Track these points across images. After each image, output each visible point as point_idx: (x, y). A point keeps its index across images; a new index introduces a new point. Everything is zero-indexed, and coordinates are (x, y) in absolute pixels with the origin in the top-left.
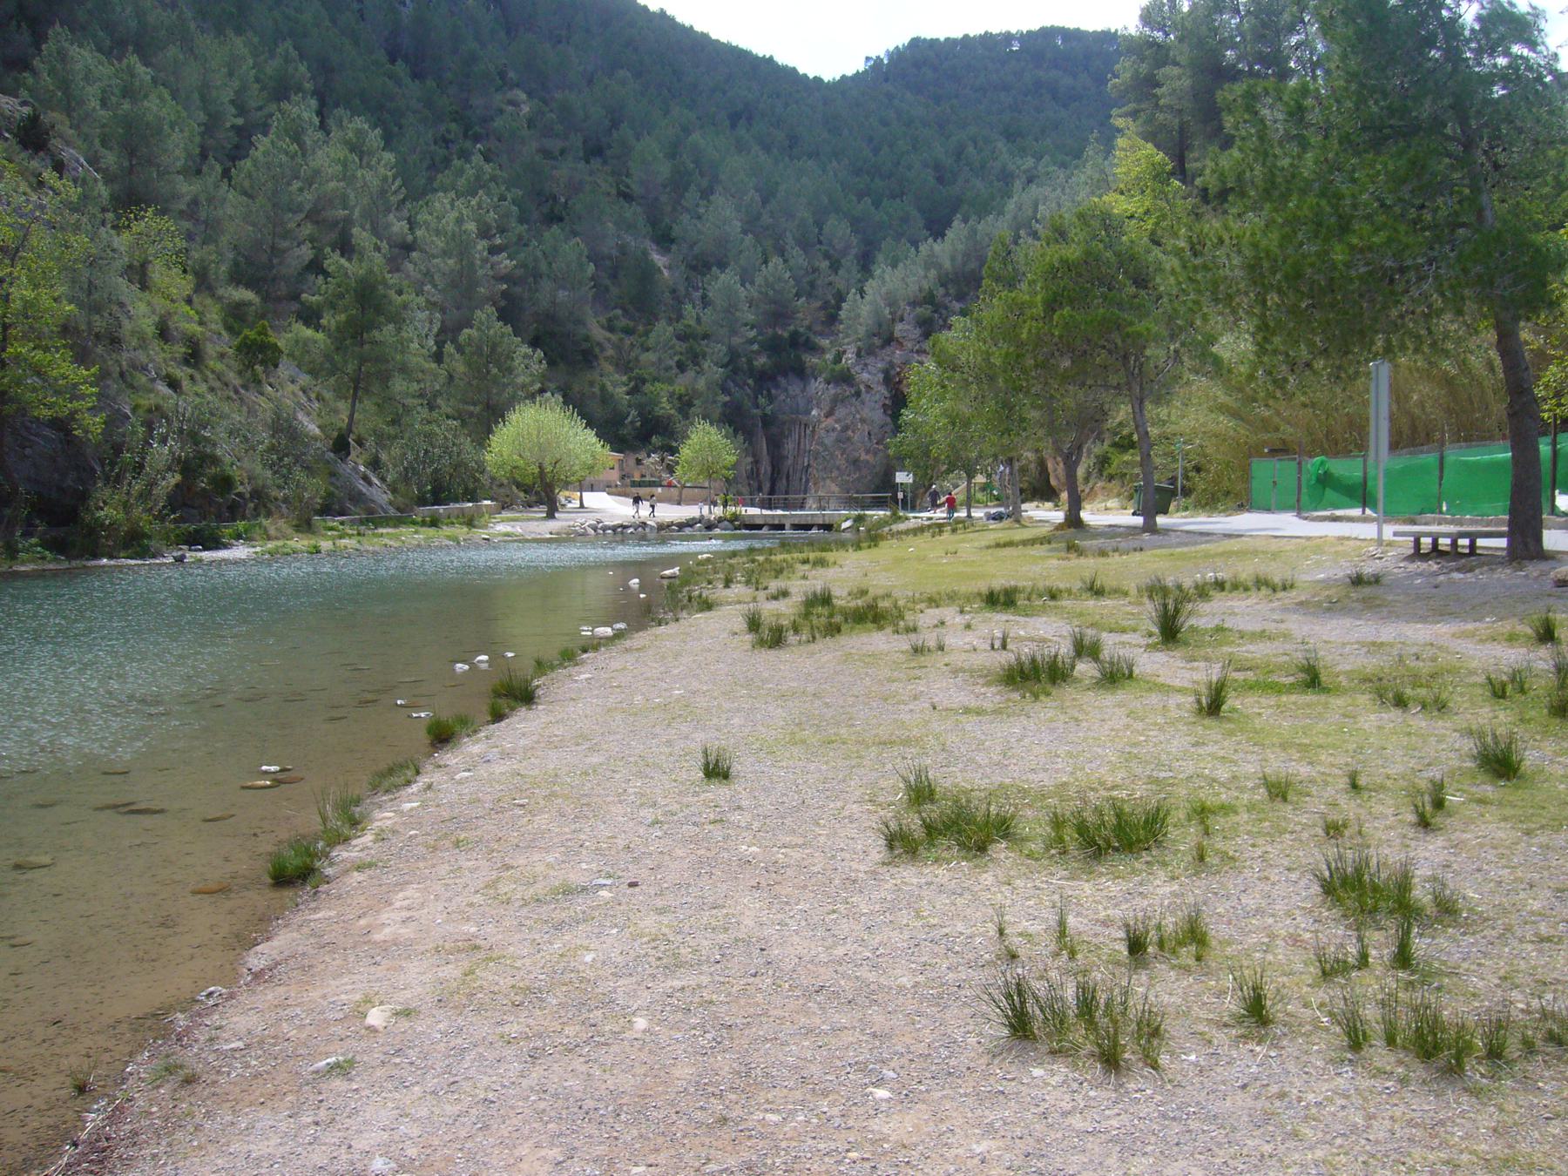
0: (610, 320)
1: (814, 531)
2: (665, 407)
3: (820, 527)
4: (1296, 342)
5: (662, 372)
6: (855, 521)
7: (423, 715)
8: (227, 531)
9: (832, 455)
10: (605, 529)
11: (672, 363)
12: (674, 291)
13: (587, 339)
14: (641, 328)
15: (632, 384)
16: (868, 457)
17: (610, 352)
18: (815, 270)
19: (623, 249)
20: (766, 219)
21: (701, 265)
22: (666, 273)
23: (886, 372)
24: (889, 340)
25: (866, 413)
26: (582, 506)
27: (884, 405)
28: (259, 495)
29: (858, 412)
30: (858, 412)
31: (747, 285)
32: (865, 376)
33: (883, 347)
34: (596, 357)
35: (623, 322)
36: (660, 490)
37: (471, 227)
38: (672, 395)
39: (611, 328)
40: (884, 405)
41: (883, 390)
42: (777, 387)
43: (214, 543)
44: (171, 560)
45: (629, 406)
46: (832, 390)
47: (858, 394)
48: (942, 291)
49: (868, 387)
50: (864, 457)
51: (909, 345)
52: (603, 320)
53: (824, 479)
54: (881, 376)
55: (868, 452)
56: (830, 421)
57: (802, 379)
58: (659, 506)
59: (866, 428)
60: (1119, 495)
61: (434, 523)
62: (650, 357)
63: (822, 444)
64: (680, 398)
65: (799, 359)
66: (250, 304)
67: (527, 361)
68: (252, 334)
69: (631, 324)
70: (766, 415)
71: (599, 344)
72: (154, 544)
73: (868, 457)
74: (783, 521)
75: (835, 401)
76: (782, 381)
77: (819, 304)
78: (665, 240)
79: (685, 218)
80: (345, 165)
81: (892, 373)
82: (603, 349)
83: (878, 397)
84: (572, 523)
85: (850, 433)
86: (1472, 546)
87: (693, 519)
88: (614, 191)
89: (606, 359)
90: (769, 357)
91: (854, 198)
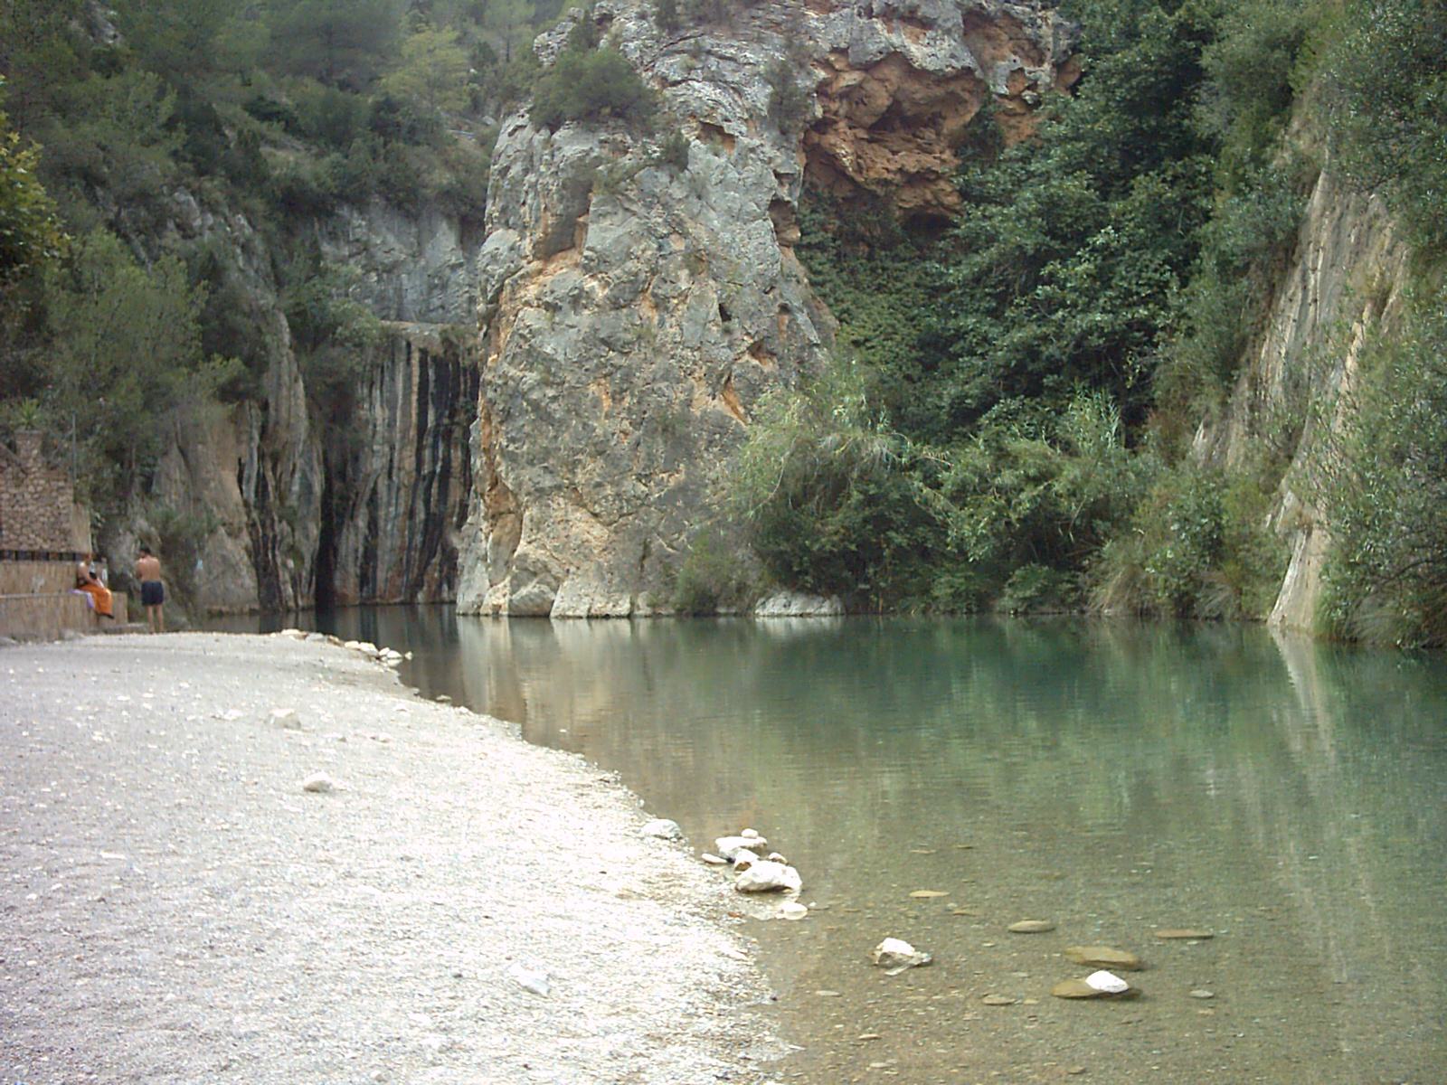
4: (1071, 35)
9: (573, 396)
16: (718, 405)
23: (780, 78)
27: (776, 204)
28: (479, 595)
29: (678, 228)
40: (776, 204)
41: (762, 142)
46: (572, 145)
47: (676, 158)
49: (713, 132)
54: (760, 95)
55: (721, 382)
56: (563, 274)
58: (649, 621)
63: (533, 357)
73: (718, 405)
83: (754, 169)
85: (645, 309)
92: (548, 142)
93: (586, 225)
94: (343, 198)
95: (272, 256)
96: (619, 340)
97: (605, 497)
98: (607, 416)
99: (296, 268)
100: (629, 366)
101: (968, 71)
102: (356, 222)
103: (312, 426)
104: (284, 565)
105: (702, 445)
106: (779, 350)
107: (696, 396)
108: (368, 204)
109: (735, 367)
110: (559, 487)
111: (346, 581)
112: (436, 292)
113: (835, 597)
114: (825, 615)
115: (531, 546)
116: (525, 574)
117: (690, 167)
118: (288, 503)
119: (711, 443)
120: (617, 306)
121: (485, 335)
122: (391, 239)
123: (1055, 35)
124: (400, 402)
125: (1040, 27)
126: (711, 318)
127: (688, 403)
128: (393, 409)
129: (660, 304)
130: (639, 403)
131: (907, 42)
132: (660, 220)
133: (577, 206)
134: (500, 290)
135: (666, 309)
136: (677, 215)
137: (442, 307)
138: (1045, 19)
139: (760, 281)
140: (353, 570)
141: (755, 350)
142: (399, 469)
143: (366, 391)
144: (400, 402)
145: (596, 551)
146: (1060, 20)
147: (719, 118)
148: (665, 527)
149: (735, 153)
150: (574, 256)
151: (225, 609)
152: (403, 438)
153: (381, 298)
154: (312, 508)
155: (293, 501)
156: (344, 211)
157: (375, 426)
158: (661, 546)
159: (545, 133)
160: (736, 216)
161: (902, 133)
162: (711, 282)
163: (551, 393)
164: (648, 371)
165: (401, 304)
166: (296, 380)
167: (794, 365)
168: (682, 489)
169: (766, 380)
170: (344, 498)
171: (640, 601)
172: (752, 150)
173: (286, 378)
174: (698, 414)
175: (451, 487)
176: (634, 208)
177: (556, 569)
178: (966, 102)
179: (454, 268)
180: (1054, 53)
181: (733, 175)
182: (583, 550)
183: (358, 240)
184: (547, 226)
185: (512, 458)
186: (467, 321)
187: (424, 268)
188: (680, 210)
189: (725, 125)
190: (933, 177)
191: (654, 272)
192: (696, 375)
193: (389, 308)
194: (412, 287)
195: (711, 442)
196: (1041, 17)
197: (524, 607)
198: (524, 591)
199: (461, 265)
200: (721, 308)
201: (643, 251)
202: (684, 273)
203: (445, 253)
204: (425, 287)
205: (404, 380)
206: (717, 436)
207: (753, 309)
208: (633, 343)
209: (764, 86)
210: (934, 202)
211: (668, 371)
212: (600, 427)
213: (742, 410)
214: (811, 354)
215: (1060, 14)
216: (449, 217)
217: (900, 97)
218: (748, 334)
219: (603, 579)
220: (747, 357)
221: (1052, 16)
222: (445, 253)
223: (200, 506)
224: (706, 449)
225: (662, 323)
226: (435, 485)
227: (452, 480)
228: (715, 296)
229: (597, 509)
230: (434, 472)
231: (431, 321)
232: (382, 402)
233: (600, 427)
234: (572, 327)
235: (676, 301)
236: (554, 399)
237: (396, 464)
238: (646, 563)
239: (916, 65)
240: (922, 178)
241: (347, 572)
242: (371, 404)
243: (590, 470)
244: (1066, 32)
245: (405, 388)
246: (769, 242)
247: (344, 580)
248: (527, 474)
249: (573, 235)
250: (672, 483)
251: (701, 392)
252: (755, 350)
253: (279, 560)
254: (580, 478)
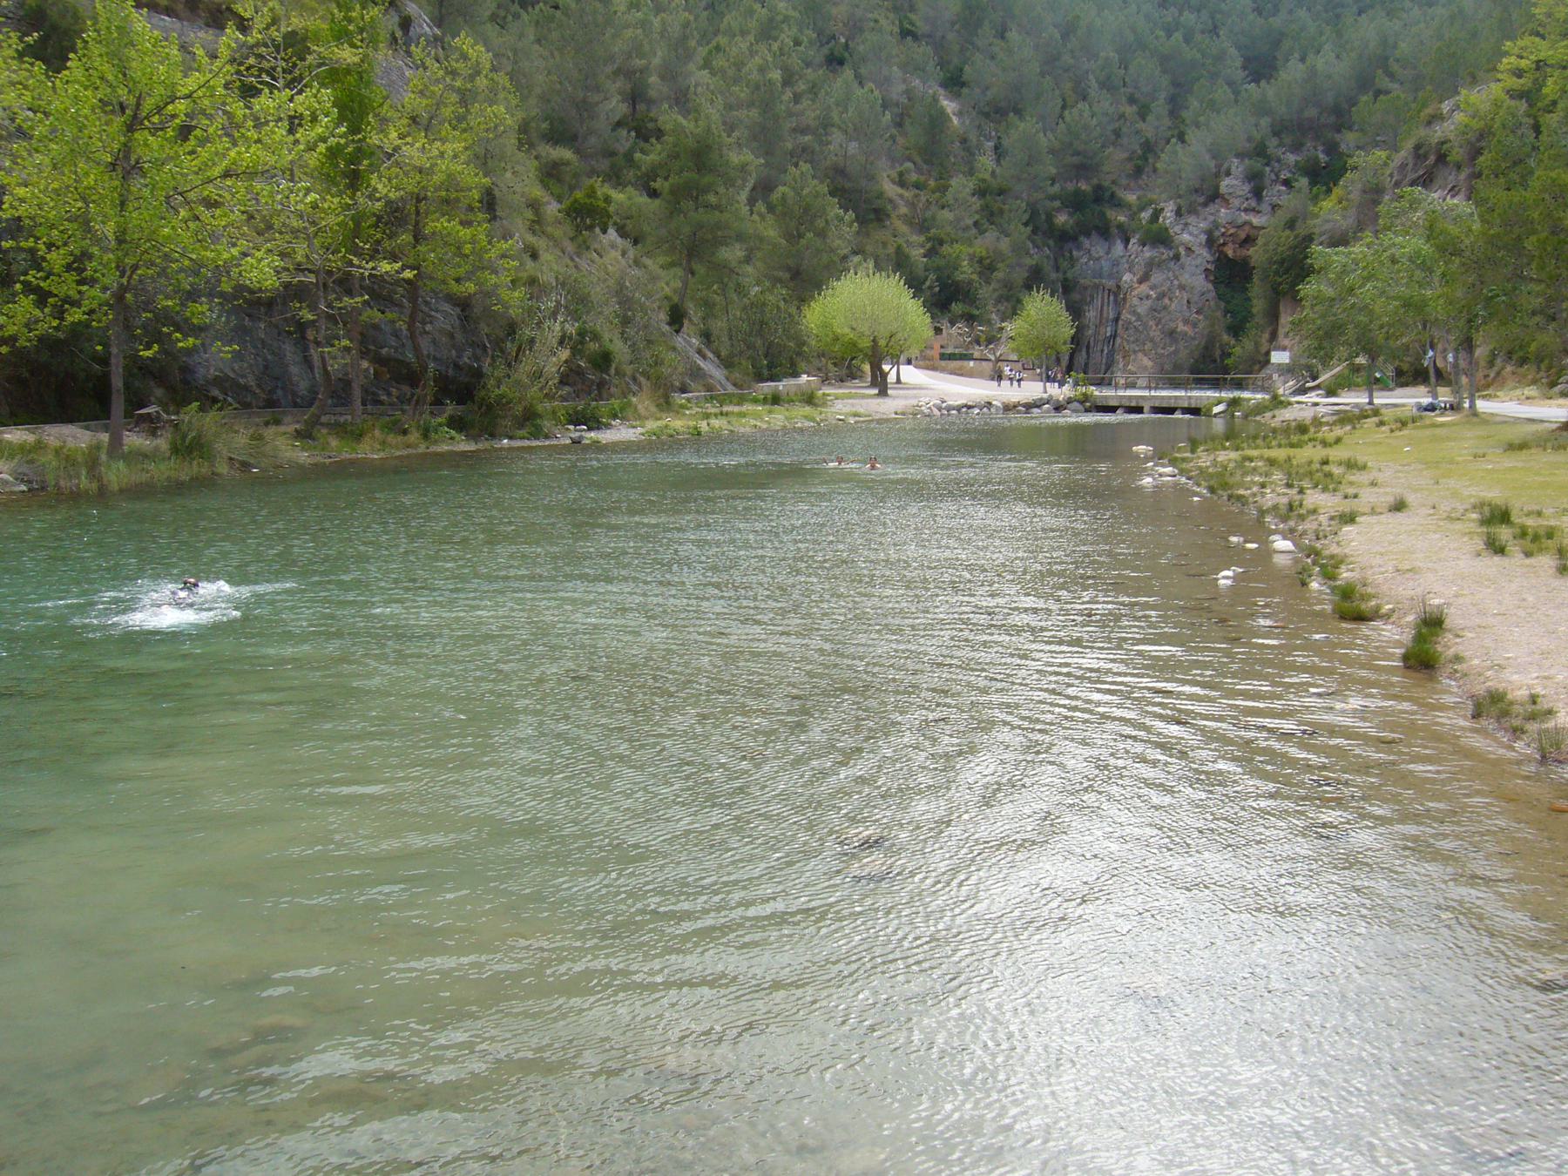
0: (901, 174)
1: (1178, 416)
2: (966, 272)
3: (1186, 411)
5: (960, 232)
6: (1228, 405)
7: (49, 604)
8: (603, 407)
9: (1145, 325)
10: (949, 408)
11: (970, 222)
12: (964, 141)
13: (880, 195)
14: (932, 183)
15: (929, 245)
16: (1186, 328)
17: (904, 210)
18: (1122, 116)
19: (909, 93)
20: (1067, 59)
21: (998, 112)
22: (955, 120)
23: (1209, 233)
24: (1214, 196)
25: (1185, 278)
26: (898, 381)
27: (1206, 270)
29: (1176, 278)
30: (1176, 278)
31: (1048, 133)
32: (1186, 237)
33: (1205, 205)
34: (888, 216)
35: (914, 177)
36: (972, 363)
37: (776, 75)
38: (972, 257)
39: (902, 183)
40: (1206, 270)
41: (1205, 253)
42: (1079, 248)
43: (594, 423)
44: (568, 441)
45: (926, 270)
46: (1148, 253)
47: (1177, 257)
48: (1274, 142)
49: (1188, 249)
50: (1181, 327)
51: (1236, 202)
52: (894, 175)
53: (1135, 352)
54: (1203, 238)
55: (1186, 322)
56: (1144, 288)
57: (1106, 239)
60: (1534, 382)
61: (776, 400)
62: (946, 215)
63: (1134, 313)
64: (981, 261)
65: (1103, 214)
66: (568, 163)
67: (842, 227)
68: (579, 194)
69: (922, 178)
70: (1066, 280)
71: (891, 201)
72: (547, 424)
73: (1186, 328)
74: (1141, 404)
75: (1151, 265)
76: (1086, 242)
77: (1125, 155)
78: (954, 83)
79: (978, 57)
81: (1217, 233)
82: (895, 207)
83: (1199, 261)
84: (915, 402)
85: (1166, 301)
87: (1041, 399)
88: (896, 30)
89: (899, 217)
90: (1070, 214)
91: (1162, 33)
99: (1064, 264)
129: (1170, 299)
141: (1197, 313)
150: (1148, 283)
156: (1082, 239)
185: (1128, 341)
212: (1152, 334)
233: (1152, 334)
243: (1148, 346)
248: (1133, 346)
252: (1197, 313)
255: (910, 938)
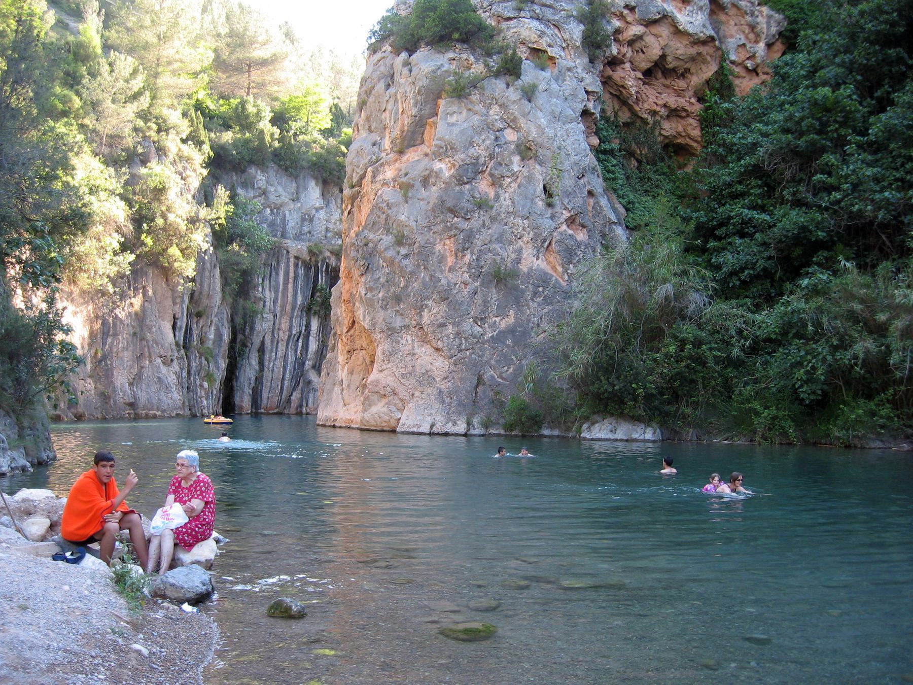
9: (425, 254)
27: (585, 113)
29: (512, 124)
30: (512, 124)
40: (585, 113)
54: (576, 31)
55: (543, 245)
59: (539, 174)
73: (541, 264)
76: (260, 178)
80: (128, 30)
83: (570, 83)
85: (483, 186)
86: (838, 135)
92: (406, 64)
93: (435, 123)
94: (251, 162)
95: (205, 192)
96: (463, 208)
97: (448, 336)
98: (451, 270)
100: (471, 229)
101: (712, 39)
102: (259, 177)
103: (223, 299)
104: (201, 386)
105: (529, 295)
106: (588, 223)
107: (524, 256)
108: (267, 168)
109: (555, 234)
110: (407, 327)
111: (244, 400)
112: (306, 223)
113: (654, 424)
114: (648, 441)
115: (382, 374)
116: (376, 396)
117: (521, 77)
118: (206, 346)
119: (535, 294)
120: (461, 183)
121: (349, 213)
122: (280, 189)
123: (768, 23)
124: (281, 288)
125: (757, 16)
126: (538, 193)
127: (518, 261)
128: (276, 292)
129: (496, 182)
130: (478, 259)
131: (675, 11)
132: (497, 118)
133: (427, 110)
134: (363, 176)
135: (501, 186)
136: (513, 114)
137: (310, 232)
138: (761, 12)
139: (576, 168)
140: (248, 391)
141: (571, 221)
142: (279, 329)
143: (260, 280)
144: (281, 288)
145: (437, 379)
146: (772, 13)
147: (544, 44)
148: (496, 361)
149: (556, 71)
151: (158, 413)
152: (282, 310)
153: (272, 225)
154: (222, 349)
155: (210, 344)
156: (252, 170)
157: (265, 302)
158: (492, 377)
159: (404, 55)
160: (556, 117)
161: (663, 80)
162: (538, 167)
163: (403, 251)
164: (485, 235)
165: (284, 228)
166: (215, 267)
167: (598, 237)
168: (511, 331)
169: (579, 247)
170: (244, 345)
171: (476, 421)
172: (569, 69)
173: (208, 265)
174: (525, 270)
175: (310, 343)
176: (476, 108)
177: (402, 393)
178: (709, 63)
179: (317, 210)
180: (767, 35)
181: (555, 86)
182: (426, 378)
183: (260, 188)
184: (403, 125)
186: (324, 242)
187: (299, 209)
188: (514, 109)
189: (549, 49)
190: (684, 114)
191: (491, 157)
192: (525, 239)
193: (277, 231)
194: (292, 221)
195: (536, 293)
196: (758, 11)
197: (373, 423)
198: (374, 409)
199: (322, 208)
200: (545, 188)
201: (484, 141)
202: (516, 159)
203: (313, 200)
204: (299, 220)
205: (287, 271)
206: (541, 289)
207: (570, 190)
208: (474, 212)
209: (578, 25)
210: (683, 134)
211: (502, 235)
212: (445, 278)
213: (560, 269)
214: (611, 230)
215: (772, 8)
216: (316, 178)
217: (668, 52)
218: (566, 209)
219: (443, 402)
220: (564, 227)
221: (765, 10)
222: (313, 200)
223: (144, 343)
224: (532, 299)
225: (497, 197)
226: (301, 341)
227: (311, 338)
228: (541, 178)
229: (440, 344)
230: (301, 332)
231: (302, 240)
232: (270, 287)
233: (445, 278)
234: (423, 200)
235: (509, 180)
236: (406, 256)
237: (277, 327)
238: (480, 389)
239: (681, 28)
240: (675, 113)
241: (243, 392)
242: (263, 288)
243: (434, 312)
244: (775, 21)
245: (284, 279)
246: (581, 140)
247: (242, 398)
249: (423, 134)
250: (503, 325)
251: (528, 252)
252: (571, 221)
253: (198, 383)
254: (426, 318)
255: (772, 164)
